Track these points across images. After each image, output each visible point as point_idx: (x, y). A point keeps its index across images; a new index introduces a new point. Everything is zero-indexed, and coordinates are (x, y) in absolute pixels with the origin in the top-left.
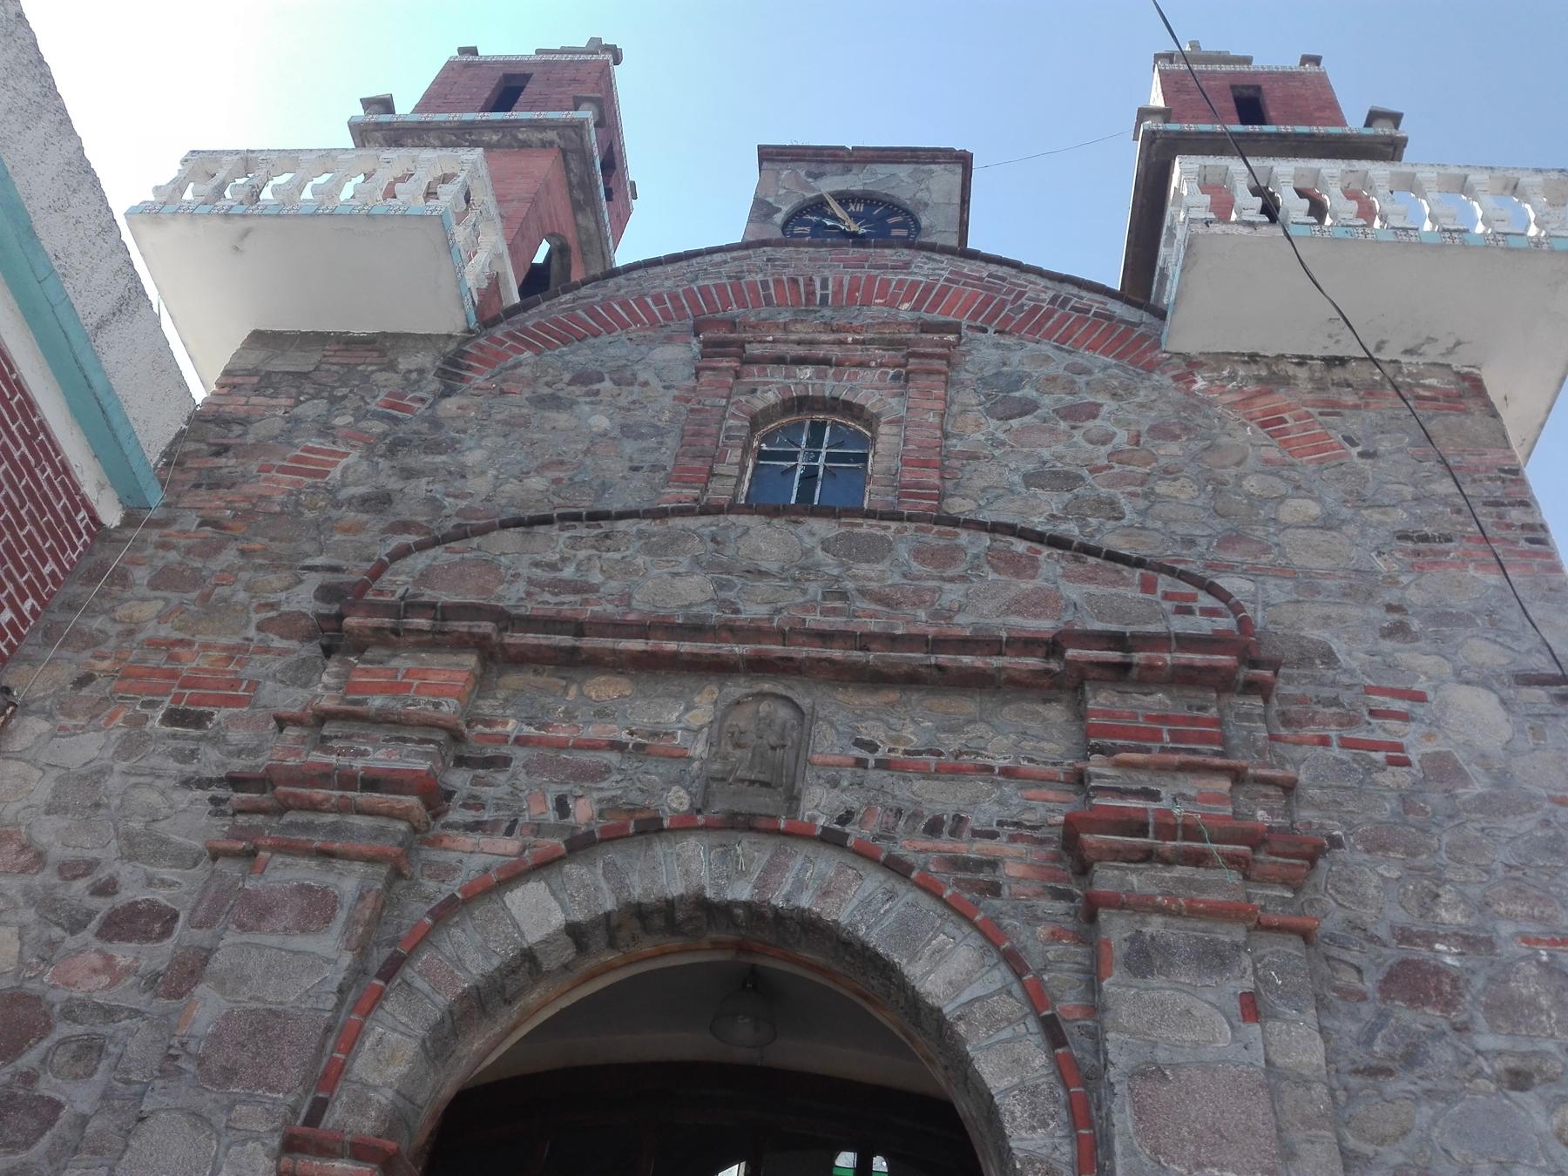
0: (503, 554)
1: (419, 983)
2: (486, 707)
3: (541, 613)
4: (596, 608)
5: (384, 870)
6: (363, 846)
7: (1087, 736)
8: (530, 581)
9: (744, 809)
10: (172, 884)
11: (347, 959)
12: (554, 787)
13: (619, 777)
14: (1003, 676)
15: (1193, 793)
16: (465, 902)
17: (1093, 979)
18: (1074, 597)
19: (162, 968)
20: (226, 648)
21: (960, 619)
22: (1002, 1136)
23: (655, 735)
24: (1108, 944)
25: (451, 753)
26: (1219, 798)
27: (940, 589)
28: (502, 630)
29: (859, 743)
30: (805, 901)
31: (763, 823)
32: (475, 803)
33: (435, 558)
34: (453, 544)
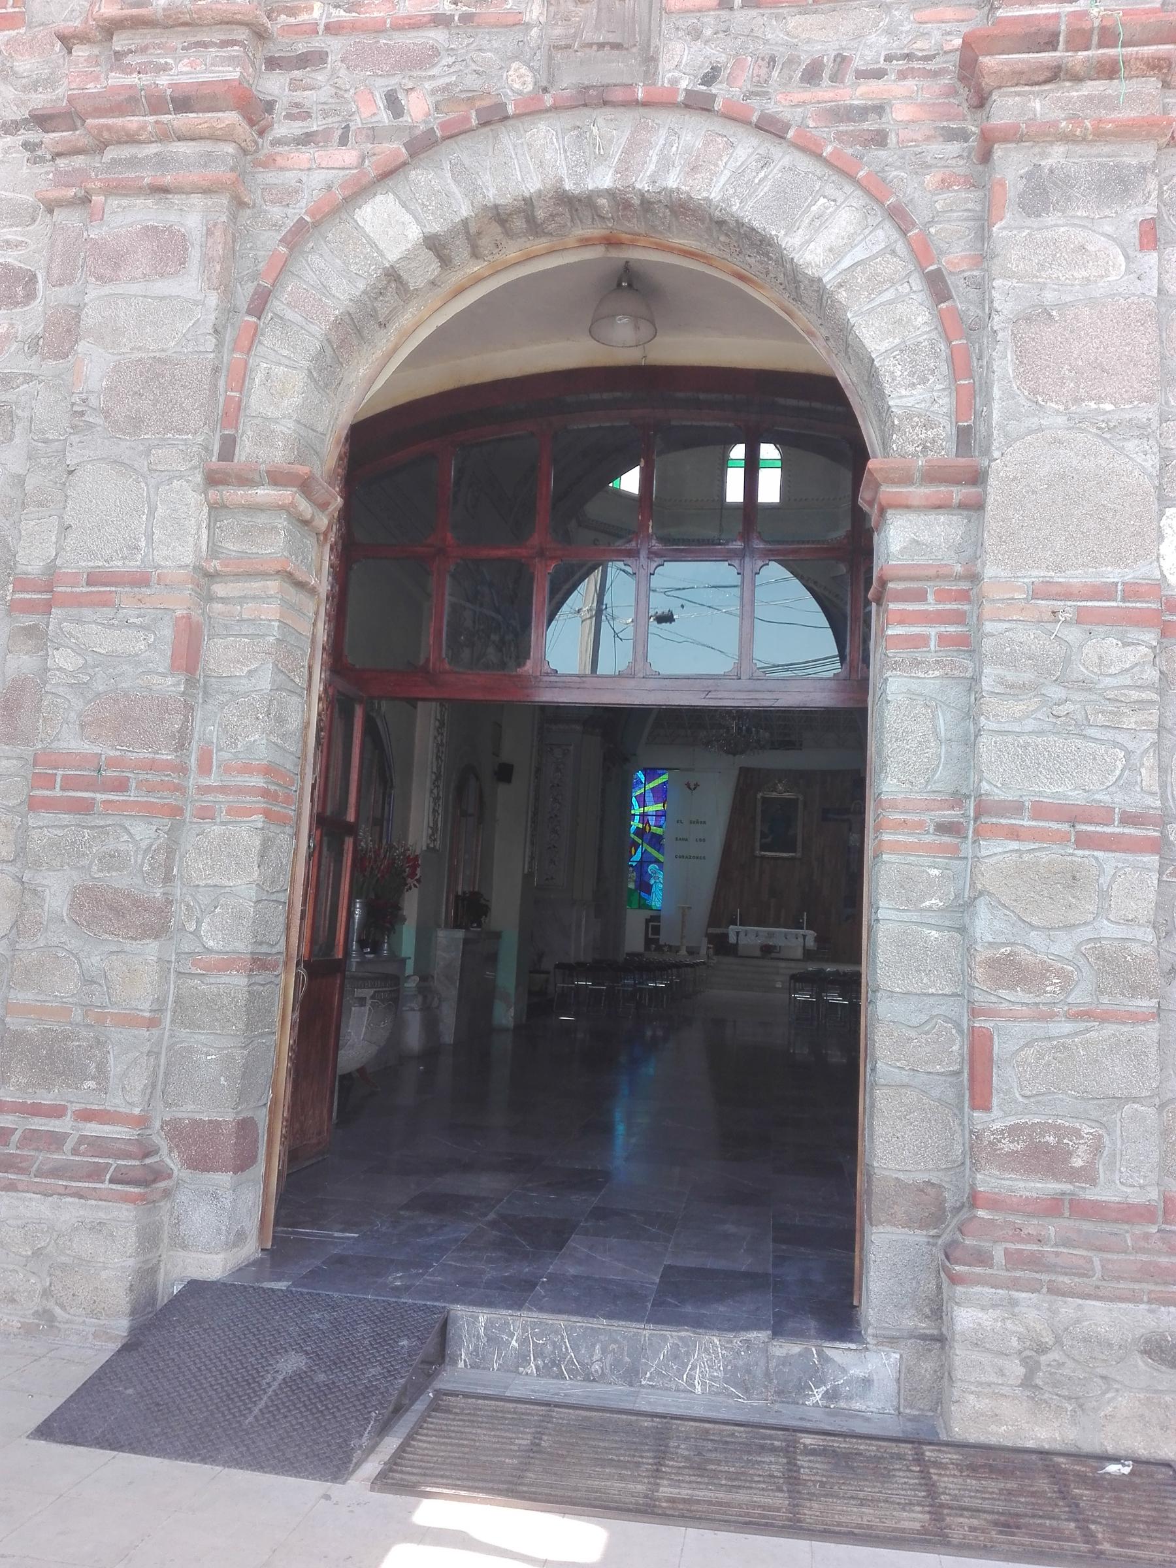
1: (290, 315)
5: (224, 200)
6: (194, 176)
9: (595, 79)
11: (213, 299)
12: (380, 82)
13: (450, 60)
19: (39, 330)
22: (881, 395)
30: (672, 181)
31: (618, 95)
32: (299, 113)
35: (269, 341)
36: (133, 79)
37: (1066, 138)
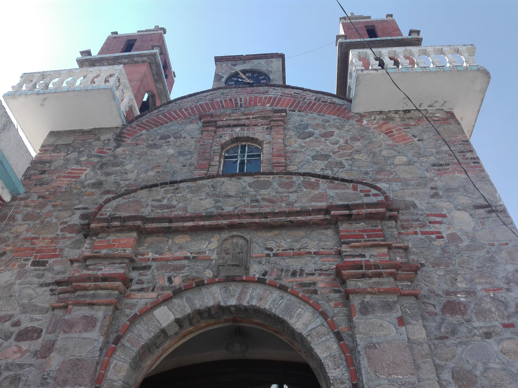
0: (142, 198)
1: (128, 344)
2: (141, 249)
3: (157, 216)
4: (175, 213)
5: (112, 308)
6: (104, 300)
7: (340, 239)
8: (152, 206)
10: (39, 320)
11: (102, 339)
12: (167, 274)
13: (188, 268)
14: (312, 222)
15: (376, 254)
16: (141, 315)
17: (350, 319)
18: (332, 194)
20: (50, 239)
21: (296, 205)
22: (325, 372)
23: (199, 253)
24: (354, 306)
25: (131, 266)
26: (384, 255)
27: (289, 196)
28: (144, 223)
29: (267, 249)
30: (254, 303)
32: (140, 282)
33: (119, 202)
34: (125, 196)
35: (118, 352)
36: (91, 272)
37: (370, 293)
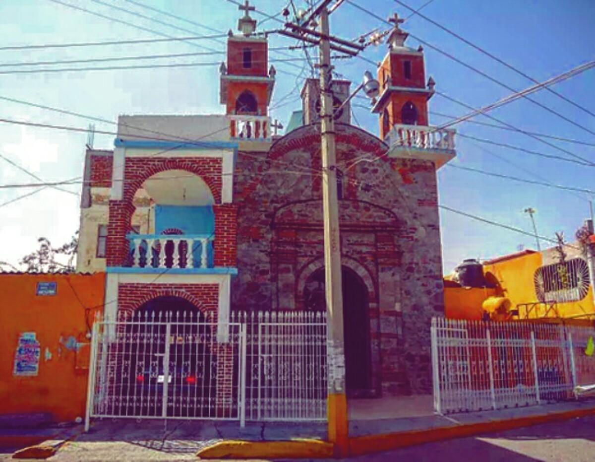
17: (377, 271)
